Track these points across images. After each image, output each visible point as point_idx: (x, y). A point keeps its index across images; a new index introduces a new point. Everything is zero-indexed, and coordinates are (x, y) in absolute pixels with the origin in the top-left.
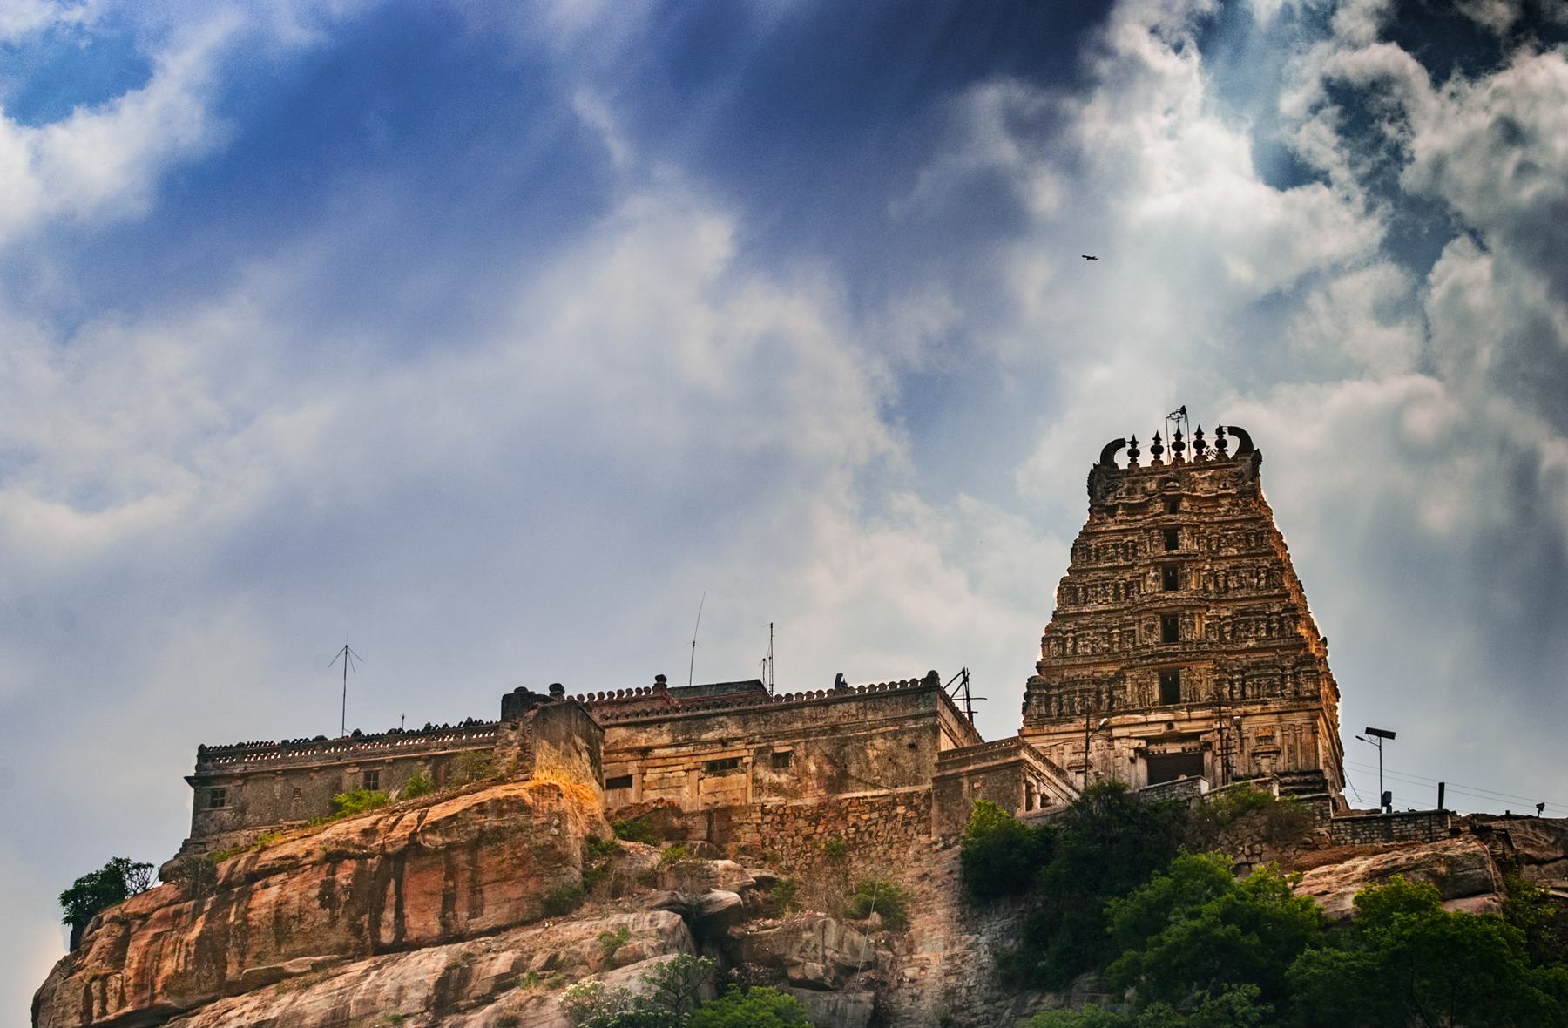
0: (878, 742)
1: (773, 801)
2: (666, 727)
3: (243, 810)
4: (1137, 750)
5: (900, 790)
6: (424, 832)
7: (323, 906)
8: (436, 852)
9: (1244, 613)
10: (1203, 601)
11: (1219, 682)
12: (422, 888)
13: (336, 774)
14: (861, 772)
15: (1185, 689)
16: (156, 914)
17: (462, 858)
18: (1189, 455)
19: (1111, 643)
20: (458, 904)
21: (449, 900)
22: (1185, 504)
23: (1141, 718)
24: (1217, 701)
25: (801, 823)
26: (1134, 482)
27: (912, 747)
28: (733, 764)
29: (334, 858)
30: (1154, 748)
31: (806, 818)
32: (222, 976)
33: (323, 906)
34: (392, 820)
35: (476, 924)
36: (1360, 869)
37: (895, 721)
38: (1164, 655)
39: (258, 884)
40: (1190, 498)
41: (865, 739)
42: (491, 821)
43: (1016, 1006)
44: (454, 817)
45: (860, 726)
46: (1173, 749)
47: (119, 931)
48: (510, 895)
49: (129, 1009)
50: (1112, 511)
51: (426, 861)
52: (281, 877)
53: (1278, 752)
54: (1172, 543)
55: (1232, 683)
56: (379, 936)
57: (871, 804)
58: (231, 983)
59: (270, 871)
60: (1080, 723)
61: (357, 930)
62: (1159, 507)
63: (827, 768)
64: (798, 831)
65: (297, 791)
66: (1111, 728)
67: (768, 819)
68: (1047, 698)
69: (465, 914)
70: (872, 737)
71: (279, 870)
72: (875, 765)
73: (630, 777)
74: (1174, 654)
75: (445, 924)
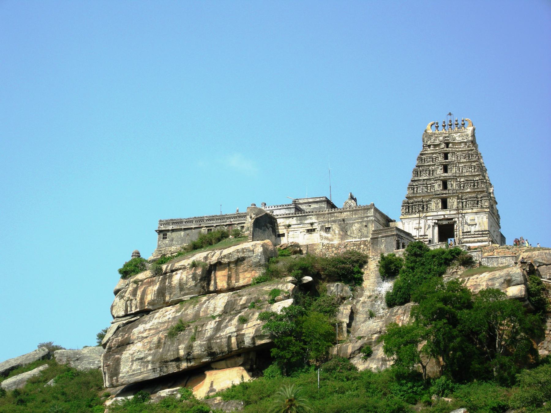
0: (356, 225)
1: (326, 242)
2: (295, 218)
3: (172, 240)
4: (435, 223)
5: (362, 239)
6: (221, 258)
7: (193, 280)
8: (225, 264)
9: (467, 181)
11: (458, 203)
13: (199, 229)
14: (351, 234)
15: (449, 205)
16: (145, 281)
17: (232, 266)
19: (427, 189)
20: (232, 279)
21: (229, 277)
22: (450, 145)
23: (435, 214)
24: (458, 209)
25: (334, 249)
26: (436, 137)
27: (366, 226)
28: (314, 230)
29: (194, 265)
30: (440, 222)
31: (335, 247)
32: (164, 300)
33: (193, 280)
34: (213, 253)
35: (237, 285)
36: (486, 277)
37: (361, 218)
38: (443, 194)
39: (174, 273)
40: (452, 143)
41: (353, 223)
42: (241, 255)
43: (391, 312)
44: (230, 254)
45: (351, 219)
46: (445, 223)
47: (135, 286)
48: (247, 276)
49: (138, 310)
50: (429, 146)
51: (222, 266)
52: (181, 271)
53: (476, 224)
54: (446, 157)
55: (462, 203)
56: (209, 288)
57: (354, 244)
58: (167, 303)
59: (177, 270)
60: (417, 215)
62: (443, 146)
63: (341, 233)
64: (333, 251)
65: (188, 234)
66: (427, 216)
67: (324, 248)
68: (412, 206)
69: (234, 282)
70: (354, 223)
71: (180, 269)
72: (355, 232)
73: (284, 234)
74: (445, 194)
75: (228, 285)
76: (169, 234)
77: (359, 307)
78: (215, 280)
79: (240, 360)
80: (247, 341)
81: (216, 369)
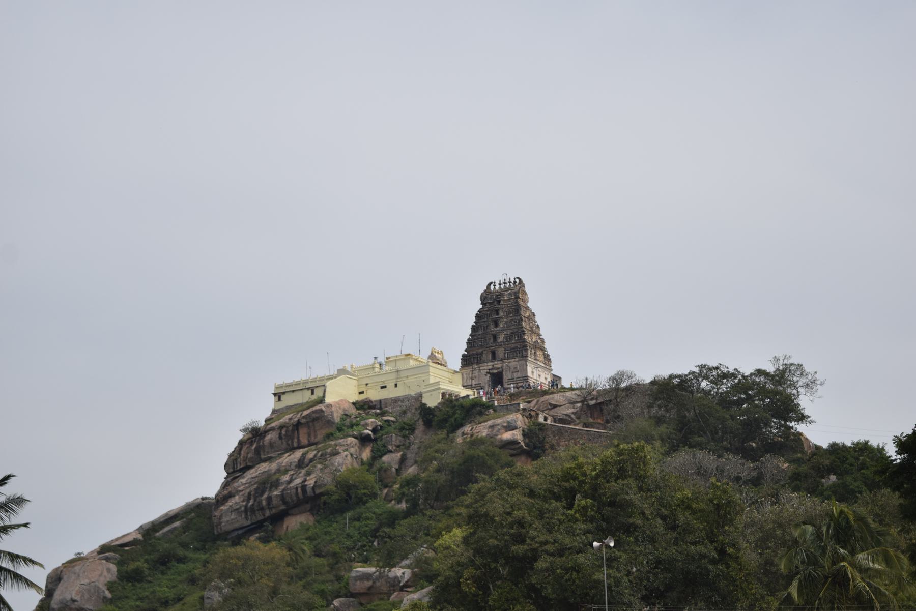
10: (502, 331)
12: (303, 432)
17: (311, 424)
18: (502, 287)
21: (309, 435)
29: (281, 427)
35: (316, 440)
46: (495, 371)
61: (288, 445)
76: (604, 407)
77: (409, 455)
78: (298, 438)
79: (308, 506)
80: (309, 491)
81: (292, 515)
